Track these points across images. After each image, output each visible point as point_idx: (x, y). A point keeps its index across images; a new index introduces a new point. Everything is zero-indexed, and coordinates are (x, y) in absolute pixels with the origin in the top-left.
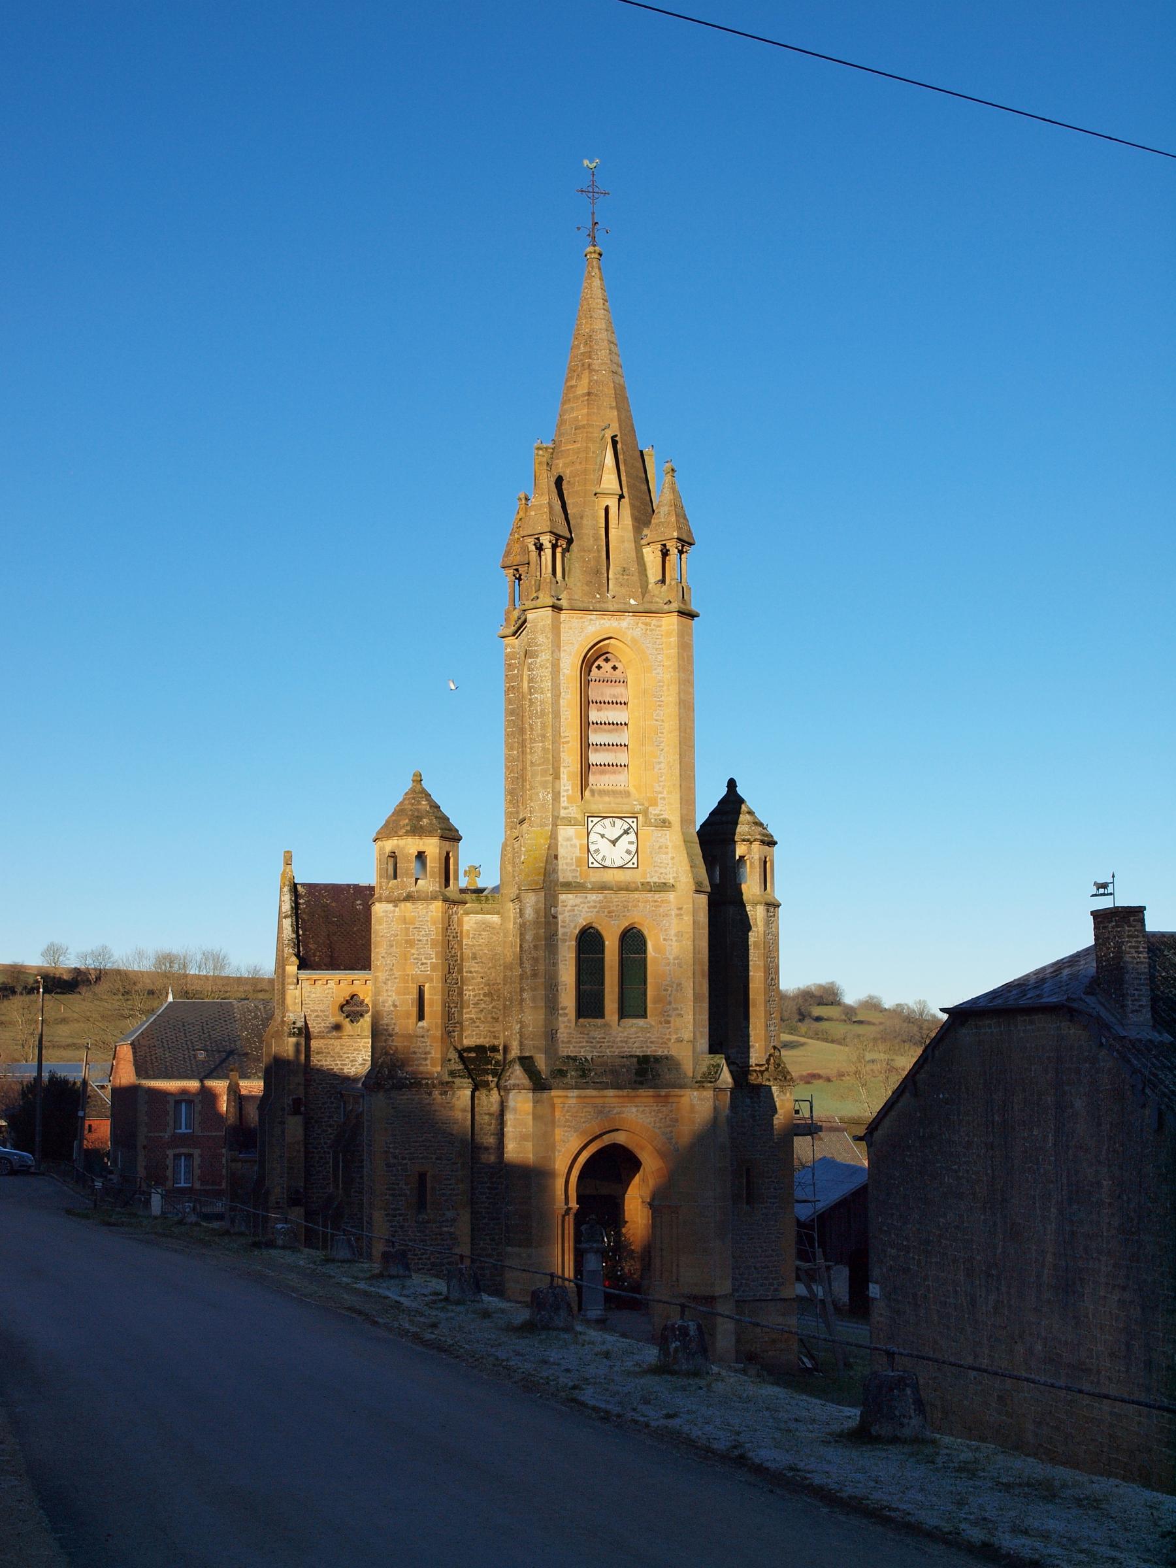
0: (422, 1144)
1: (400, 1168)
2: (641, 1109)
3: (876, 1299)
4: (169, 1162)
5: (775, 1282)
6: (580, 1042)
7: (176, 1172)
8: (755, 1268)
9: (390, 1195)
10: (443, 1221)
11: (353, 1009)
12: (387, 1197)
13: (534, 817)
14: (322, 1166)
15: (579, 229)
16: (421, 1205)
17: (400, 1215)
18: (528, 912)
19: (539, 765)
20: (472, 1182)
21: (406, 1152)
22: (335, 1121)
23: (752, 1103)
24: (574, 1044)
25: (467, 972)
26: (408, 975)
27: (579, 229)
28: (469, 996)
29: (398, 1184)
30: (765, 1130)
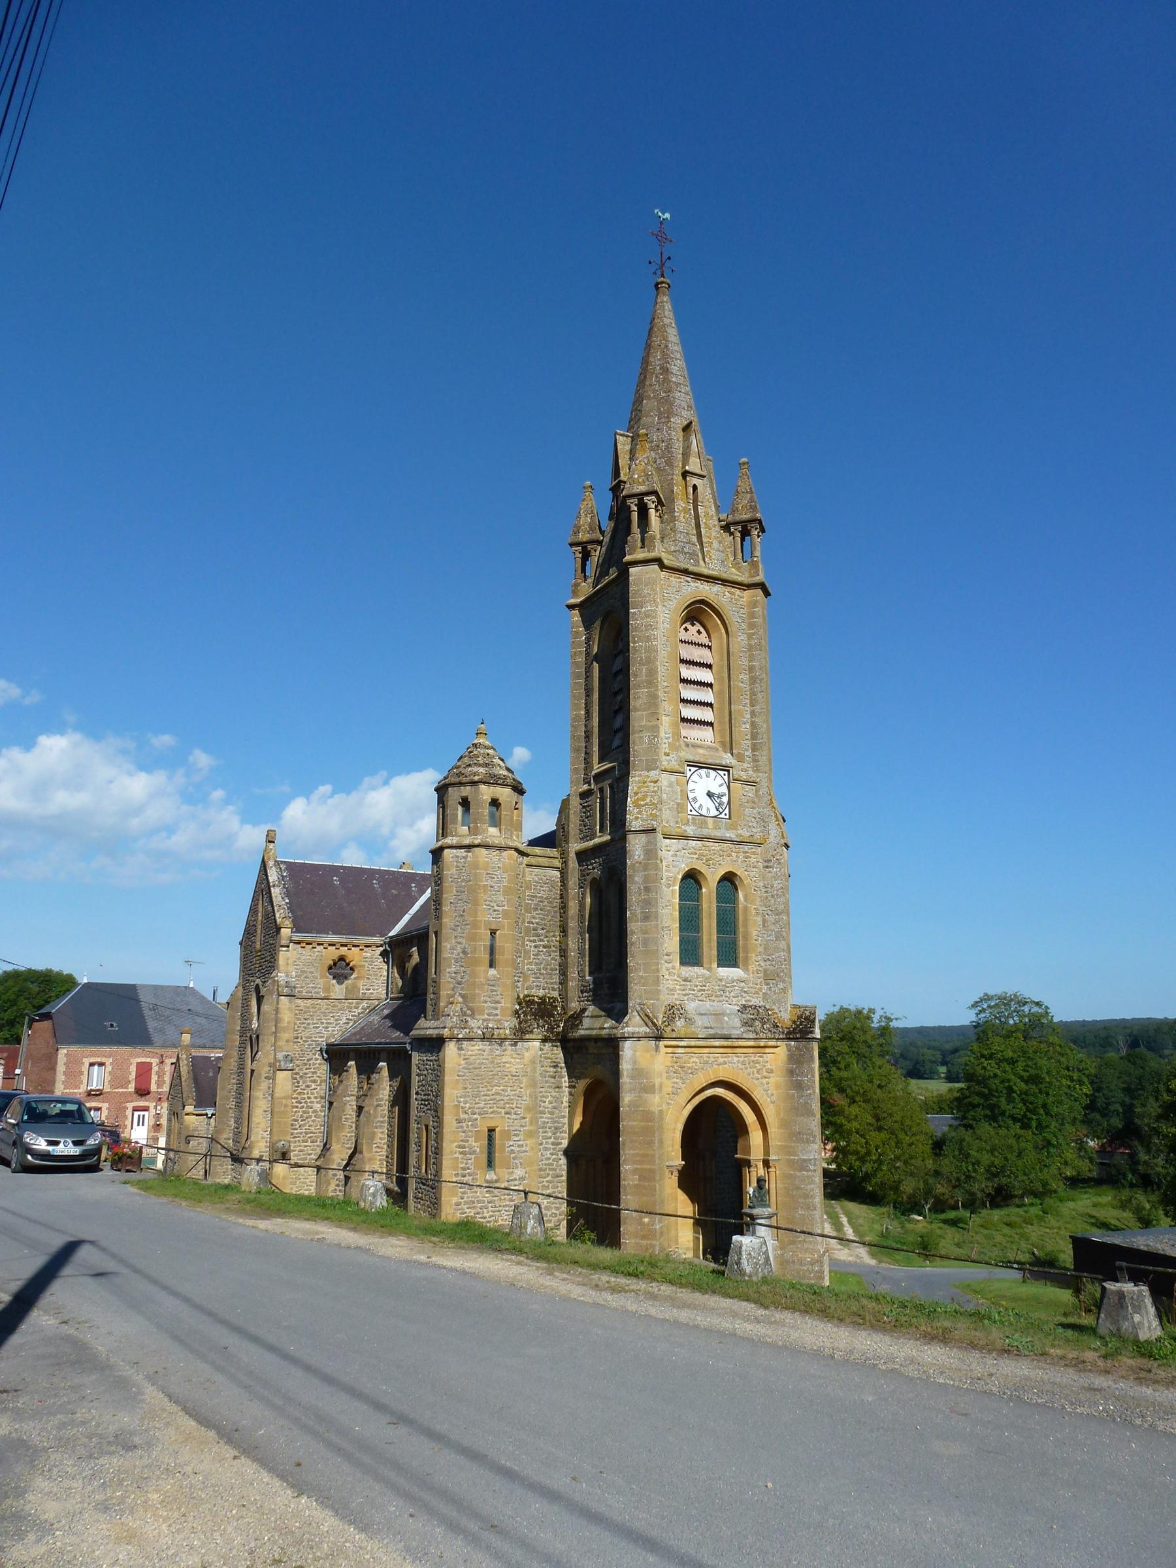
0: (492, 1097)
1: (470, 1123)
2: (742, 1059)
6: (683, 990)
9: (461, 1153)
10: (512, 1180)
11: (338, 971)
13: (638, 760)
14: (304, 1120)
15: (650, 263)
17: (470, 1175)
18: (637, 853)
19: (644, 710)
22: (319, 1077)
29: (468, 1141)
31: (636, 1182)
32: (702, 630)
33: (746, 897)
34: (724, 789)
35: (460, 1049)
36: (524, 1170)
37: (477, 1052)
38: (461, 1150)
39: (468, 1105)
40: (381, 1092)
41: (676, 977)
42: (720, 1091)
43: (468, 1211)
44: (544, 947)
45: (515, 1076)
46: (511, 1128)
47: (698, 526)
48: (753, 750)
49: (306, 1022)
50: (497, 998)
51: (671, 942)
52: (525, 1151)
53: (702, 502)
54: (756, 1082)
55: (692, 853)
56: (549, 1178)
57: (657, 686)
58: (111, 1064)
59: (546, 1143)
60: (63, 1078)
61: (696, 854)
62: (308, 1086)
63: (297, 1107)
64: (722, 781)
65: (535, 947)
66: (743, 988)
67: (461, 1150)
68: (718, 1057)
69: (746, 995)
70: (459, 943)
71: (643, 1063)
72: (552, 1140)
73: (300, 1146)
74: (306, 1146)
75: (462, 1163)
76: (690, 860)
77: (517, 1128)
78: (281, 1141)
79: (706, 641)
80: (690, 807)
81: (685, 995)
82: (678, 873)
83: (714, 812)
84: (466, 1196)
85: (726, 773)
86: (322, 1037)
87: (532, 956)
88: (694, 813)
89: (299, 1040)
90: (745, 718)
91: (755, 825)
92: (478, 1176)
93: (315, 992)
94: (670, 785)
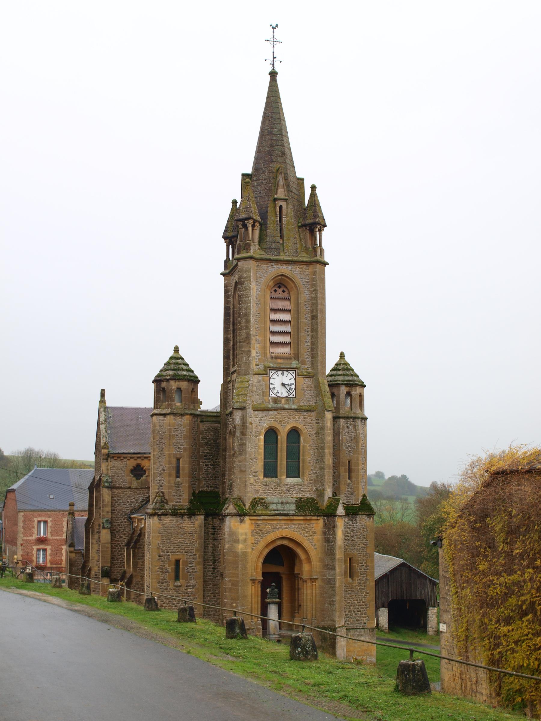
1: (165, 557)
2: (297, 526)
3: (444, 632)
4: (34, 552)
5: (364, 619)
7: (38, 558)
8: (354, 612)
9: (161, 572)
10: (188, 586)
12: (159, 573)
14: (119, 556)
16: (177, 578)
18: (237, 420)
20: (204, 565)
21: (169, 548)
22: (127, 532)
23: (353, 523)
24: (261, 491)
25: (202, 453)
26: (171, 454)
27: (266, 60)
28: (203, 465)
29: (164, 566)
30: (359, 538)
31: (230, 587)
32: (285, 289)
33: (304, 440)
34: (293, 381)
35: (160, 520)
36: (195, 581)
37: (169, 521)
38: (161, 570)
39: (164, 548)
40: (141, 541)
41: (259, 484)
42: (286, 543)
43: (165, 600)
44: (211, 465)
45: (190, 533)
46: (188, 560)
47: (281, 230)
48: (312, 357)
49: (119, 501)
50: (181, 494)
51: (259, 466)
52: (196, 572)
53: (286, 215)
54: (305, 538)
55: (271, 418)
56: (211, 586)
57: (250, 329)
58: (51, 521)
59: (209, 568)
60: (22, 530)
61: (273, 418)
62: (121, 537)
63: (115, 548)
64: (292, 377)
65: (206, 465)
66: (301, 489)
67: (161, 570)
68: (282, 525)
69: (303, 492)
70: (161, 465)
71: (234, 529)
72: (213, 566)
73: (117, 570)
74: (121, 570)
75: (162, 577)
76: (270, 422)
77: (191, 560)
78: (105, 566)
79: (286, 295)
80: (271, 393)
81: (265, 493)
82: (262, 429)
83: (285, 394)
84: (164, 593)
85: (294, 372)
86: (128, 510)
87: (204, 471)
88: (274, 395)
89: (115, 511)
90: (307, 339)
91: (311, 399)
92: (170, 583)
93: (123, 485)
94: (259, 382)
